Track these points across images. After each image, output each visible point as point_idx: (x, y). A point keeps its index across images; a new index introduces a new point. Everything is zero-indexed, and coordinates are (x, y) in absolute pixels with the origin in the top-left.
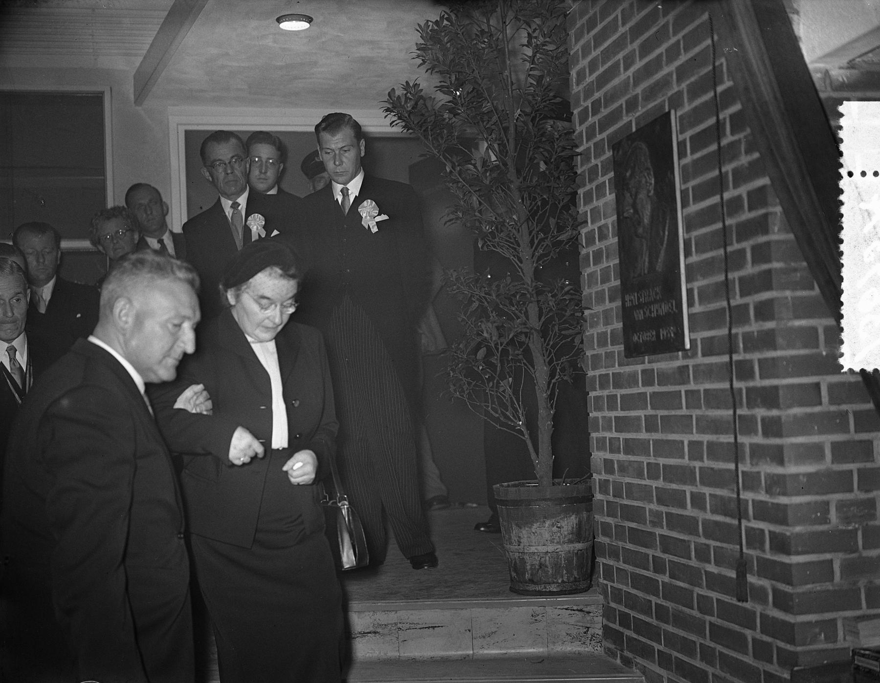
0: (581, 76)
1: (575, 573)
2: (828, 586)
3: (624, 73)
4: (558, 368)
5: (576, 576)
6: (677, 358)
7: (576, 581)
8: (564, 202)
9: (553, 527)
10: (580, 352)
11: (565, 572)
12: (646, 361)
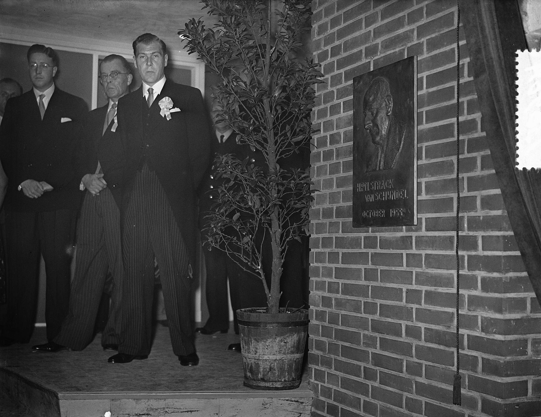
0: (322, 29)
1: (293, 375)
2: (524, 399)
3: (365, 28)
4: (291, 231)
5: (294, 377)
6: (401, 231)
7: (293, 380)
8: (303, 115)
9: (282, 342)
10: (306, 221)
11: (287, 374)
12: (370, 231)
